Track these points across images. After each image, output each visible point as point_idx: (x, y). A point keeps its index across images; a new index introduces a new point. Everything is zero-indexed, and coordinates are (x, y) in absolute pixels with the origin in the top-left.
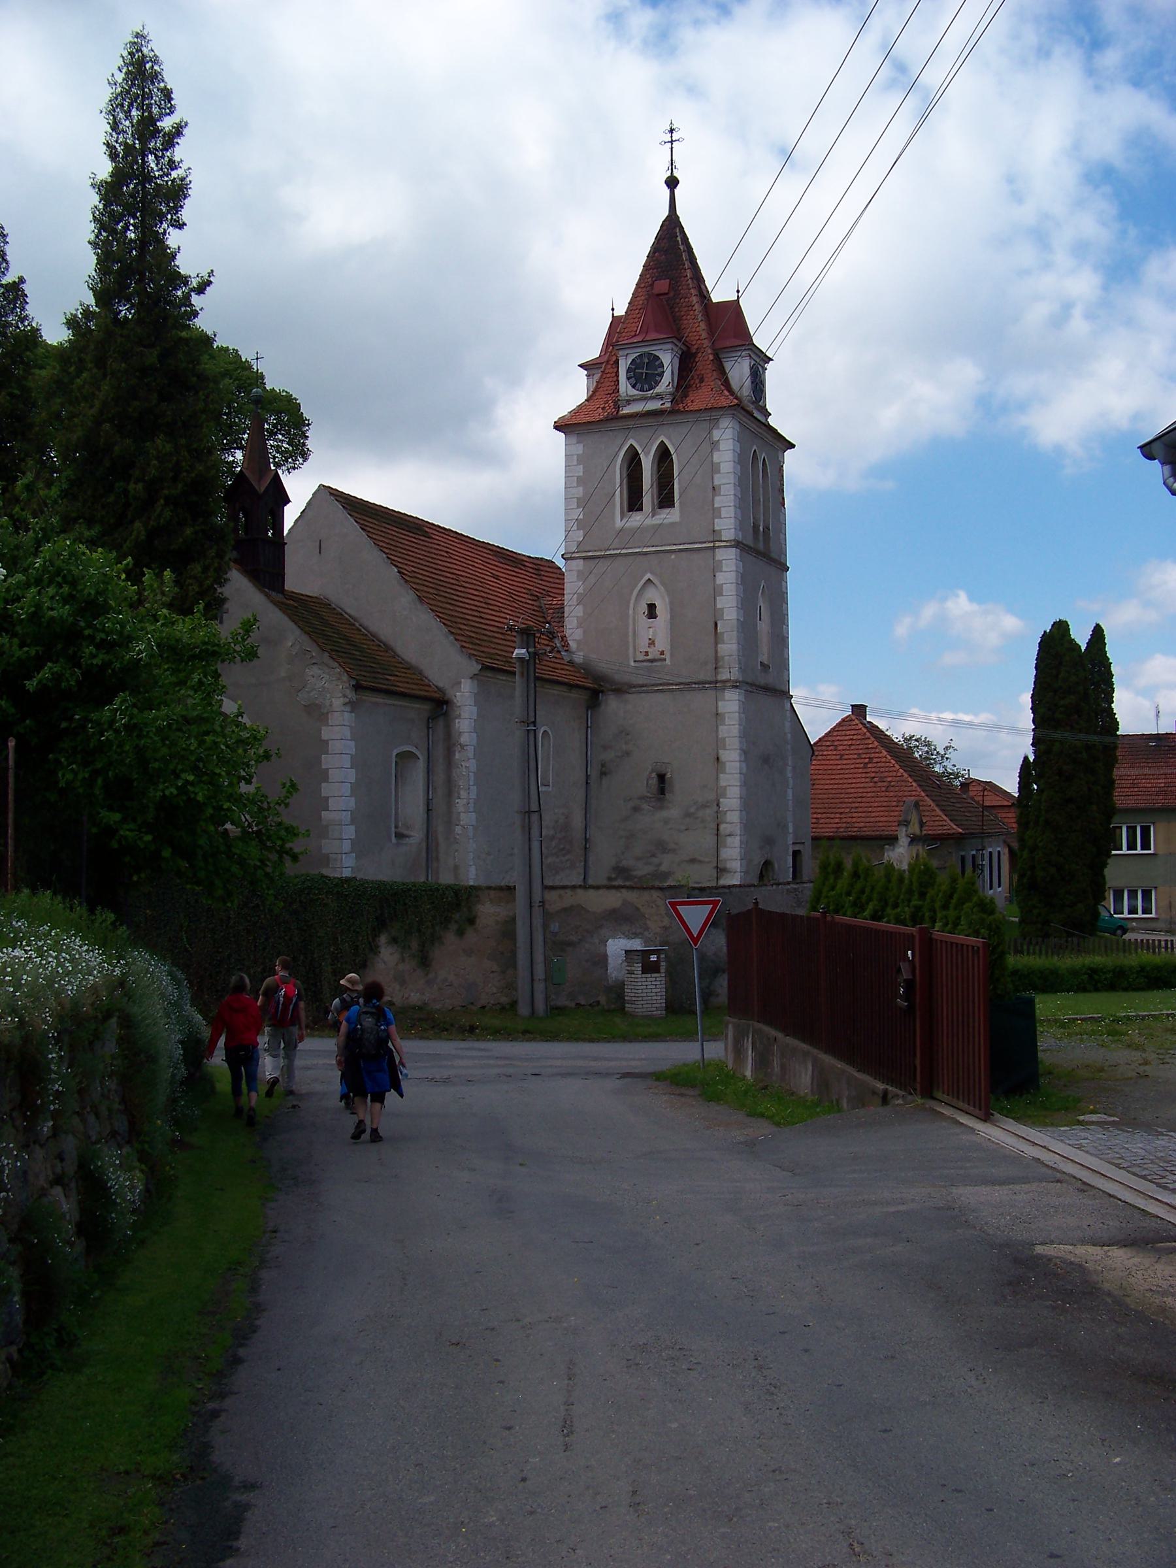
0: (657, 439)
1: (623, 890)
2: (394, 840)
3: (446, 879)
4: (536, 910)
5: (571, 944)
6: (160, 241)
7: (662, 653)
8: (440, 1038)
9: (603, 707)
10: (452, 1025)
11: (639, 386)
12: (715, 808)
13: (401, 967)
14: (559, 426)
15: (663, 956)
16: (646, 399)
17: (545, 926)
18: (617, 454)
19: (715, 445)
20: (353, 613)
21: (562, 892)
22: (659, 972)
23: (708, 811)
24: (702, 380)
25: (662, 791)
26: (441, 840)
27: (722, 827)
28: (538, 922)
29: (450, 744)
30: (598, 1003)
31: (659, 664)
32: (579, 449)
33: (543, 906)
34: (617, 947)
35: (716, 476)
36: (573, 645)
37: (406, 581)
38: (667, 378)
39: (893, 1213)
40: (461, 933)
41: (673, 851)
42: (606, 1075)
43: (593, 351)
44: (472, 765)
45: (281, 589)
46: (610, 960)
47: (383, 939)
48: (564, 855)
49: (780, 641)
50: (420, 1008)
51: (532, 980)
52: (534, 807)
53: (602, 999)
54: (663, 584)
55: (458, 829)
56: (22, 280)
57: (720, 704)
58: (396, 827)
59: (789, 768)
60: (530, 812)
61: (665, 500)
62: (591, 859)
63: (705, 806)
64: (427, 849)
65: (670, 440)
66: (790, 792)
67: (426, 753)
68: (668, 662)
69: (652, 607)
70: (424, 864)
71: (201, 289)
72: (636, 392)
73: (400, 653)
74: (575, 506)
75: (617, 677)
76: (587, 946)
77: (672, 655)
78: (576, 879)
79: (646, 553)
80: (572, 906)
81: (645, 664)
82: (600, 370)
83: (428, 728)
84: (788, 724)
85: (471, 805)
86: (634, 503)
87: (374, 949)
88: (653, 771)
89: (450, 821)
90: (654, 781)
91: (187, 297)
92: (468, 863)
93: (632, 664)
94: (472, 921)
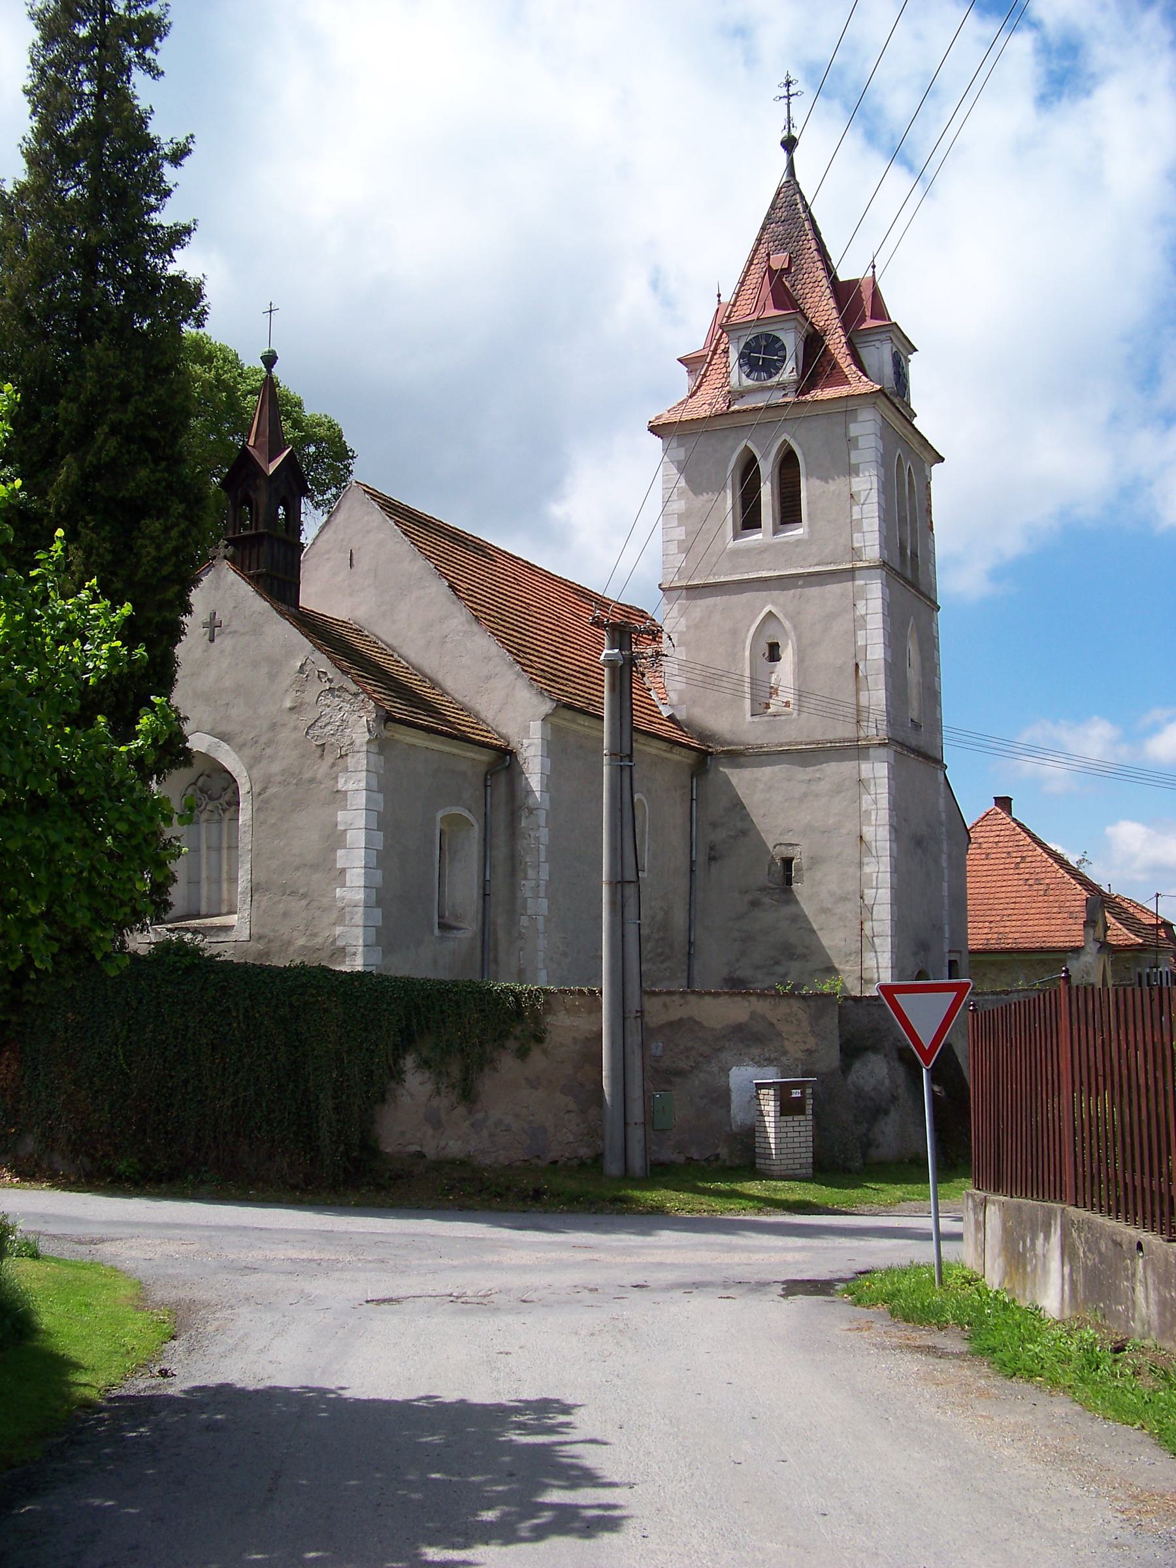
2: (436, 931)
4: (633, 1025)
5: (680, 1073)
6: (124, 98)
8: (490, 1209)
10: (508, 1188)
13: (435, 1103)
14: (654, 429)
15: (809, 1091)
17: (644, 1045)
19: (852, 443)
21: (667, 999)
22: (803, 1113)
26: (501, 935)
27: (867, 926)
28: (635, 1039)
30: (717, 1156)
32: (681, 454)
33: (642, 1017)
34: (742, 1076)
38: (790, 365)
39: (199, 893)
40: (522, 1054)
41: (804, 957)
42: (761, 1286)
44: (544, 834)
45: (297, 606)
46: (734, 1096)
47: (409, 1062)
48: (662, 962)
49: (932, 695)
50: (462, 1163)
51: (626, 1124)
52: (630, 875)
53: (723, 1152)
55: (524, 921)
59: (944, 856)
61: (789, 512)
62: (697, 967)
63: (844, 899)
65: (793, 436)
66: (945, 885)
67: (482, 821)
70: (478, 967)
71: (179, 155)
74: (675, 523)
76: (702, 1075)
80: (681, 1019)
83: (486, 786)
84: (941, 801)
85: (542, 888)
86: (750, 520)
87: (397, 1075)
91: (156, 166)
94: (539, 1039)
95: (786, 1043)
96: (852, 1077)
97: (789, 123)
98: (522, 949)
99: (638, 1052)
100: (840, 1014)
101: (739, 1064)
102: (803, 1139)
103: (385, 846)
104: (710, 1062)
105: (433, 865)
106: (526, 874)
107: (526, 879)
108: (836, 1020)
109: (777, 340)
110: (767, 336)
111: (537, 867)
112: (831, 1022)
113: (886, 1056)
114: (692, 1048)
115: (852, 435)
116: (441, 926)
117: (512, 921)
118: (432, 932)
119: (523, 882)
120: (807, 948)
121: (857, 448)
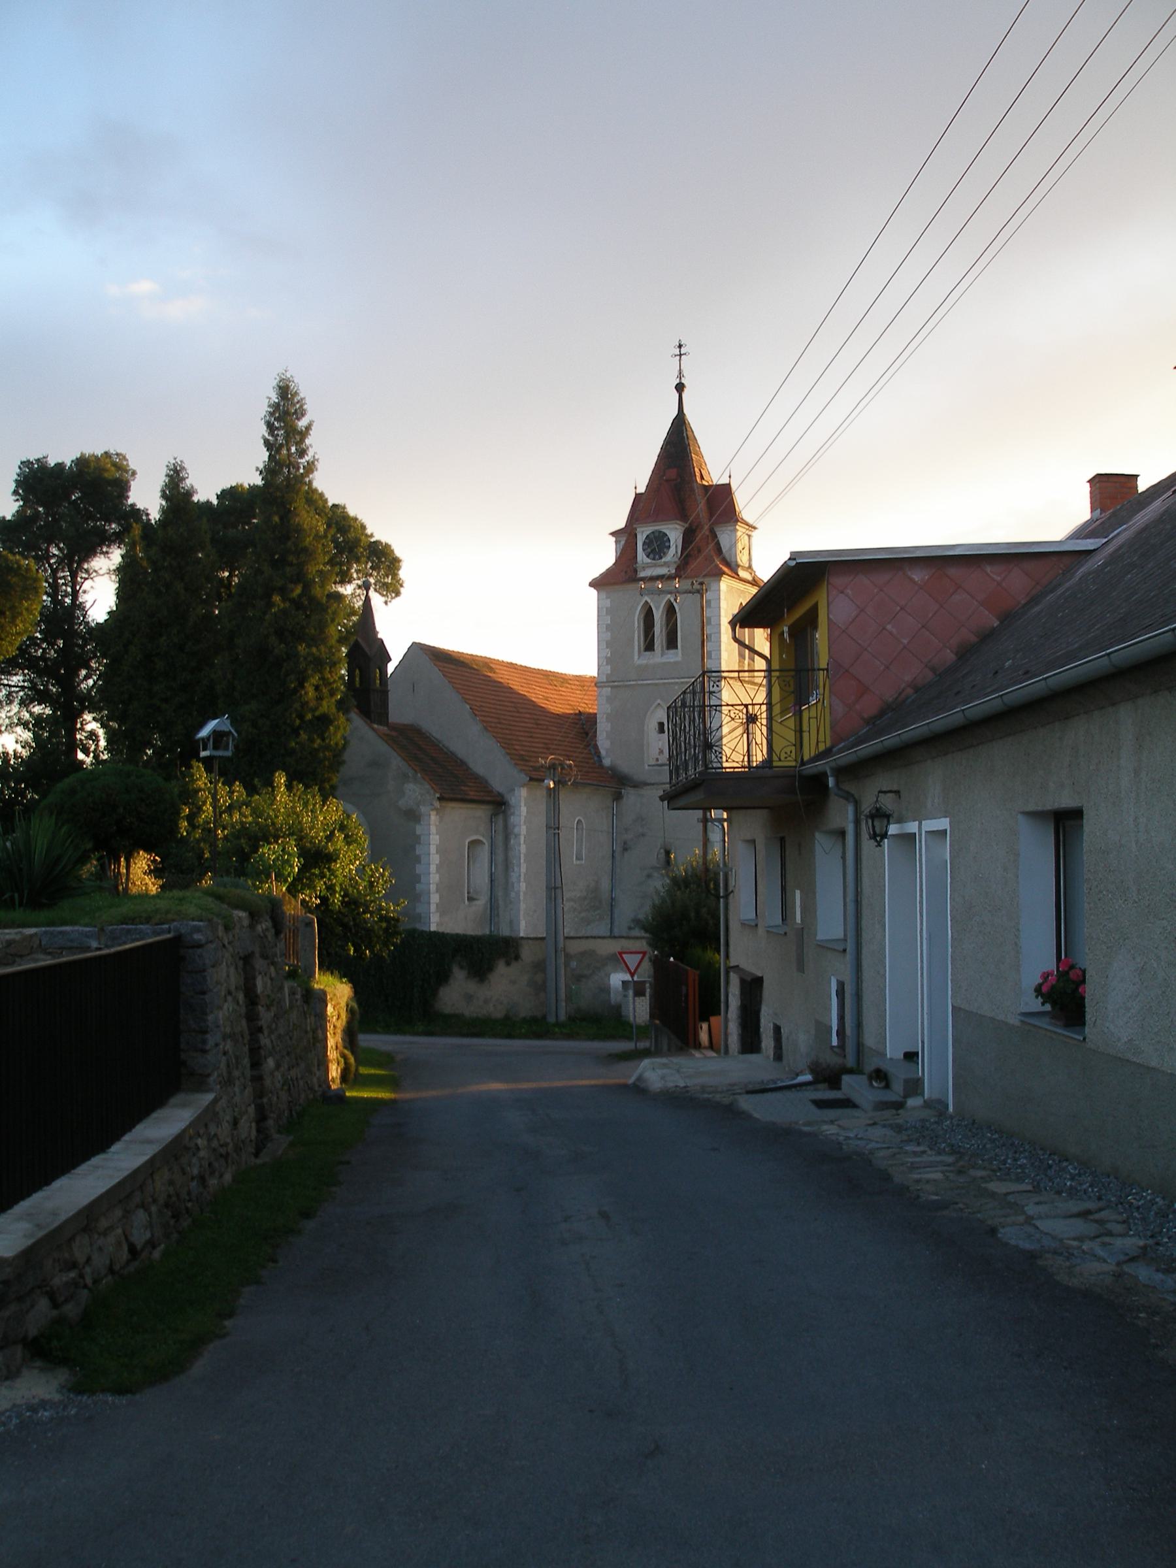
3: (505, 932)
16: (655, 566)
17: (567, 965)
20: (437, 736)
26: (501, 903)
28: (562, 960)
29: (507, 833)
36: (603, 753)
38: (672, 551)
43: (621, 524)
44: (523, 848)
55: (513, 895)
56: (175, 476)
60: (555, 888)
61: (672, 643)
78: (603, 930)
79: (656, 684)
82: (625, 537)
86: (649, 646)
89: (507, 887)
90: (662, 856)
92: (525, 919)
101: (615, 971)
111: (519, 866)
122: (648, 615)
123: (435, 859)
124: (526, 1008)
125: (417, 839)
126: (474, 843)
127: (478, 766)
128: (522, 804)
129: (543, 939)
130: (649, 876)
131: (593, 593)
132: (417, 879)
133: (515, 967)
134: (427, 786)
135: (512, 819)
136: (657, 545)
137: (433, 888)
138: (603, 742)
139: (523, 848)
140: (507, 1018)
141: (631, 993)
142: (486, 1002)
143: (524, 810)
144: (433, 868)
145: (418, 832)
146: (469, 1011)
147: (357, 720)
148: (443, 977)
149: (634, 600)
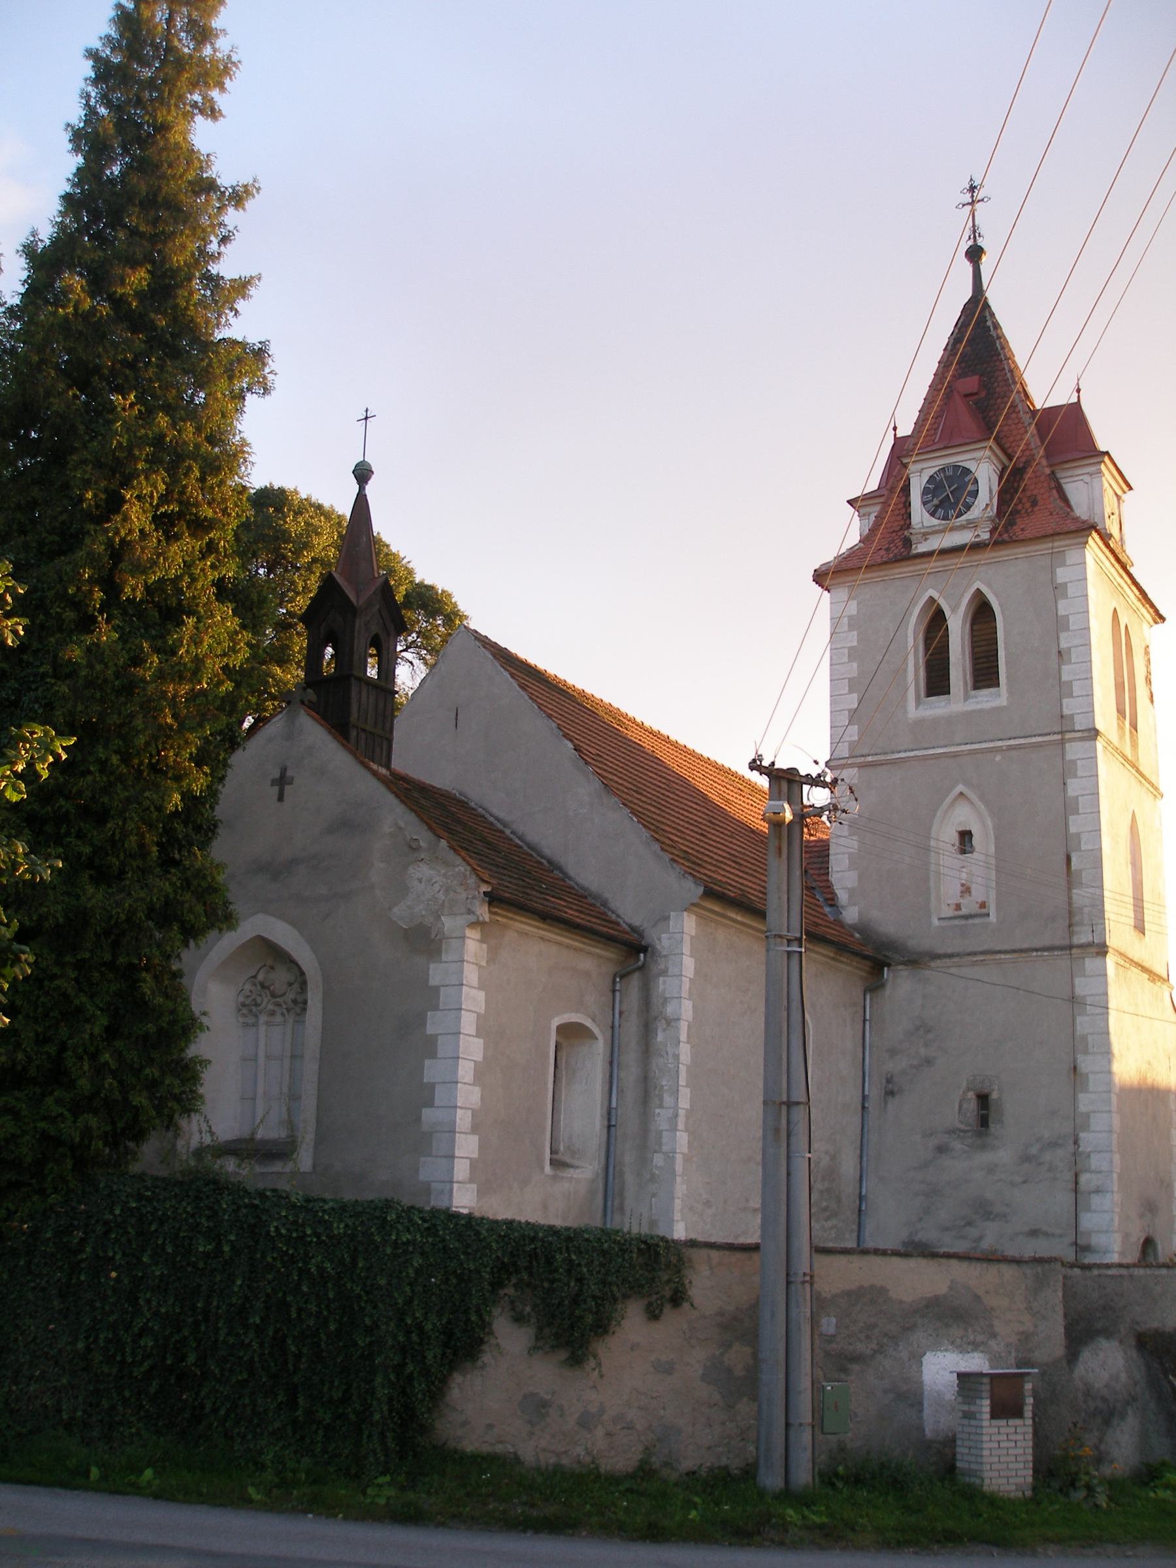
0: (969, 586)
1: (954, 1262)
2: (548, 1169)
5: (857, 1358)
7: (983, 905)
9: (888, 990)
11: (941, 512)
12: (1071, 1148)
17: (814, 1323)
18: (907, 613)
20: (501, 814)
22: (1019, 1414)
23: (1060, 1152)
24: (1034, 503)
25: (984, 1122)
26: (630, 1178)
27: (1084, 1178)
29: (650, 1018)
31: (977, 921)
35: (1063, 635)
36: (842, 897)
37: (587, 763)
38: (983, 498)
41: (1003, 1217)
44: (685, 1052)
54: (982, 798)
55: (658, 1160)
57: (1077, 981)
58: (553, 1151)
60: (790, 1104)
61: (985, 673)
63: (1054, 1145)
64: (606, 1191)
65: (989, 586)
68: (993, 918)
69: (965, 837)
71: (239, 197)
72: (935, 522)
73: (572, 873)
75: (911, 943)
77: (998, 908)
79: (955, 755)
81: (956, 922)
83: (614, 991)
86: (937, 682)
88: (969, 1089)
89: (646, 1141)
90: (972, 1105)
92: (695, 1192)
93: (936, 922)
95: (996, 1322)
96: (1080, 1370)
97: (974, 232)
98: (654, 1195)
99: (806, 1328)
100: (1064, 1284)
101: (936, 1347)
102: (1021, 1451)
103: (485, 1058)
104: (897, 1344)
105: (546, 1084)
106: (661, 1099)
107: (661, 1106)
108: (1060, 1294)
109: (967, 471)
110: (956, 467)
111: (676, 1092)
112: (1054, 1296)
113: (1121, 1342)
114: (875, 1325)
115: (1059, 581)
116: (552, 1162)
117: (644, 1160)
118: (543, 1169)
119: (657, 1111)
120: (1007, 1205)
121: (1065, 597)
122: (936, 621)
123: (472, 1048)
124: (697, 1446)
125: (431, 997)
126: (571, 1033)
127: (587, 872)
128: (686, 949)
129: (755, 1248)
130: (942, 1149)
131: (821, 602)
132: (425, 1096)
133: (673, 1322)
134: (462, 868)
135: (663, 985)
136: (950, 494)
137: (463, 1119)
138: (843, 875)
139: (685, 1052)
140: (644, 1471)
141: (985, 1405)
142: (586, 1422)
143: (689, 964)
144: (465, 1071)
145: (434, 980)
146: (534, 1448)
147: (313, 733)
148: (464, 1344)
149: (906, 597)
